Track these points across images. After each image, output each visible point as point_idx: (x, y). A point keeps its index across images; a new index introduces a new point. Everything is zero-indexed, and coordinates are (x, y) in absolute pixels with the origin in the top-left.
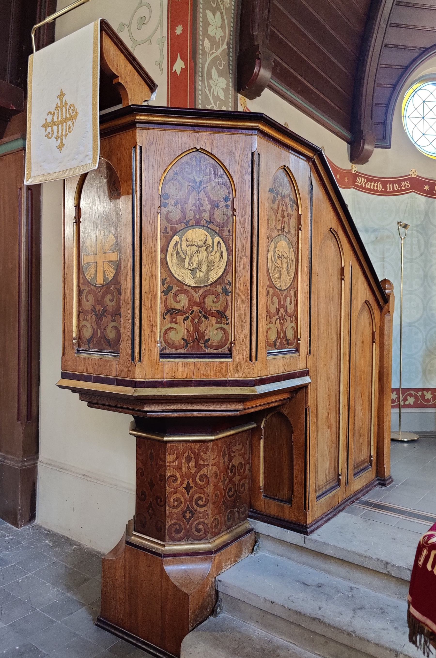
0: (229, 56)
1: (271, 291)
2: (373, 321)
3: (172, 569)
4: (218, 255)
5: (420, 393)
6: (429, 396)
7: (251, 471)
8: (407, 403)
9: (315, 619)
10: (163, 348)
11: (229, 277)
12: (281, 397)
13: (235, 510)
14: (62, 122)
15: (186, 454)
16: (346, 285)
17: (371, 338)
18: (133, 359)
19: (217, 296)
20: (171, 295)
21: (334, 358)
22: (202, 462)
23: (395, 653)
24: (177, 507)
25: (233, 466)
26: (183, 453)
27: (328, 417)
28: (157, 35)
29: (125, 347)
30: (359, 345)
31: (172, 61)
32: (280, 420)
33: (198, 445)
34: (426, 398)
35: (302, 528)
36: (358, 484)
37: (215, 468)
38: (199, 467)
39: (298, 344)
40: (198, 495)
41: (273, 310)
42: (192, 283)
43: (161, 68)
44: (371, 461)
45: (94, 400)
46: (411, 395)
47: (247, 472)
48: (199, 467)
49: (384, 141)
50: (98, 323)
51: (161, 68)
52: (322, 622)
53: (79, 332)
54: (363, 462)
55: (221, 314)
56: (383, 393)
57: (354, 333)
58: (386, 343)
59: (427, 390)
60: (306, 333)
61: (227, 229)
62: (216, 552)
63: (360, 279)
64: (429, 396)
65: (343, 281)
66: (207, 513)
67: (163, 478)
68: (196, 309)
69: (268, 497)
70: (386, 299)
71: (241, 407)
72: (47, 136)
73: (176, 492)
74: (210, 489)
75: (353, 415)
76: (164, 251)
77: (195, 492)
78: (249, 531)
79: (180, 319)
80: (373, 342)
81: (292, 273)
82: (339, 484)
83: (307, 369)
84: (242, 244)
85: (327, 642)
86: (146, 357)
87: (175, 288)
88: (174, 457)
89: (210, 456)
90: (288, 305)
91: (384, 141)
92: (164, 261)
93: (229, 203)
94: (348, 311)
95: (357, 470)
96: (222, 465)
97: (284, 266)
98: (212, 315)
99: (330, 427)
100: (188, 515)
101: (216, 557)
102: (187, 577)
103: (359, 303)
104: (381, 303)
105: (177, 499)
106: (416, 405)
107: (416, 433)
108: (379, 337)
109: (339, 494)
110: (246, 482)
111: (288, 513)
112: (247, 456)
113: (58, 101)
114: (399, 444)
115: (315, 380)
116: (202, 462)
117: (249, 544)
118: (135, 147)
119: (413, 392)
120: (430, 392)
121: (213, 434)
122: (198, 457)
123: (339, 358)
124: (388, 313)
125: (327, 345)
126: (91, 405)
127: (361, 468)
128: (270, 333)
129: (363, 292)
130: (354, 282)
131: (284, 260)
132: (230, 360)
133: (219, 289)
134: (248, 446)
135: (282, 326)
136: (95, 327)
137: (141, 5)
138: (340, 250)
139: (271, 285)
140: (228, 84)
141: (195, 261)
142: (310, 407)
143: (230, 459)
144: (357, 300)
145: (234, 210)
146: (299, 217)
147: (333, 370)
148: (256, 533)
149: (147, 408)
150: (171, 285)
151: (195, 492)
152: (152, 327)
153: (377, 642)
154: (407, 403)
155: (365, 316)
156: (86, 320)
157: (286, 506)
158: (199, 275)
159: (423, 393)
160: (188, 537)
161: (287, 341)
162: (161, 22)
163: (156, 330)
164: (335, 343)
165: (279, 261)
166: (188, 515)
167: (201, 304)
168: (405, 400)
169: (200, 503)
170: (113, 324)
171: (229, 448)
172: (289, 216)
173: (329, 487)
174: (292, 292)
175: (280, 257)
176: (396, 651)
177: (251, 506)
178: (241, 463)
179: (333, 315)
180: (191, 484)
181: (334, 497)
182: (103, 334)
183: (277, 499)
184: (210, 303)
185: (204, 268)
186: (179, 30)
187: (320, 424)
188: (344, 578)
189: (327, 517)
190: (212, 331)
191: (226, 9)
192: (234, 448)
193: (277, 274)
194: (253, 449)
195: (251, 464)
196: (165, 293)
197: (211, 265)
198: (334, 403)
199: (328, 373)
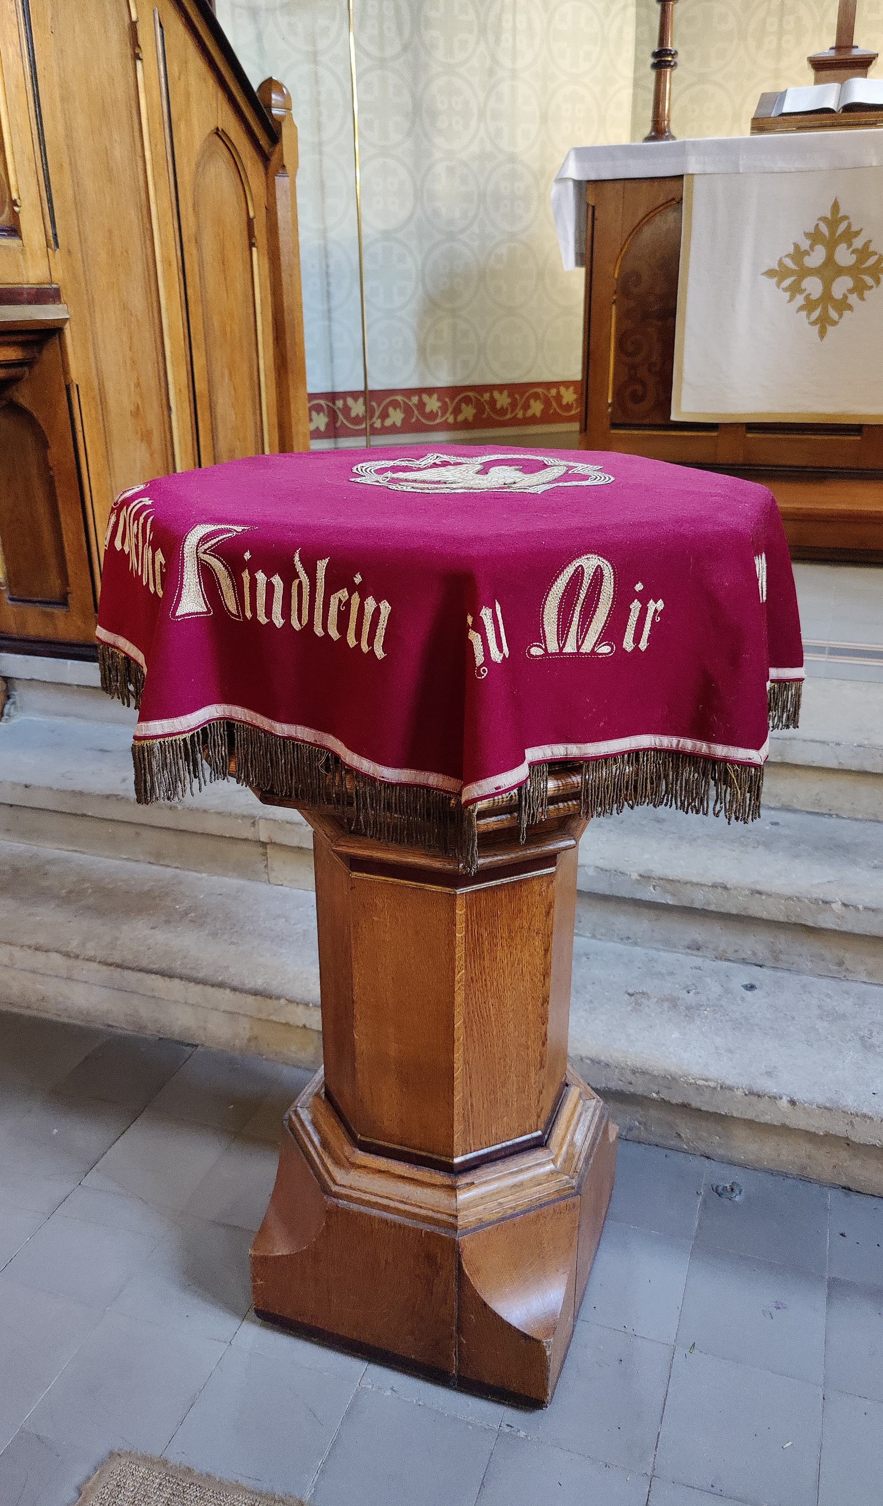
2: (246, 188)
5: (415, 399)
6: (433, 404)
8: (388, 422)
9: (108, 797)
16: (148, 72)
17: (245, 233)
21: (138, 269)
23: (252, 821)
27: (137, 413)
34: (428, 410)
46: (395, 404)
52: (122, 798)
56: (286, 372)
57: (190, 210)
59: (430, 391)
60: (34, 189)
63: (191, 65)
65: (139, 63)
69: (19, 601)
75: (207, 414)
80: (252, 245)
83: (54, 286)
85: (138, 834)
94: (163, 148)
99: (146, 437)
104: (263, 141)
108: (266, 234)
119: (399, 398)
120: (435, 396)
123: (152, 273)
125: (110, 232)
129: (204, 108)
142: (76, 382)
144: (188, 122)
147: (138, 300)
153: (221, 810)
154: (388, 422)
155: (220, 174)
157: (58, 611)
159: (420, 400)
168: (385, 415)
176: (253, 817)
179: (120, 153)
183: (39, 602)
199: (125, 307)
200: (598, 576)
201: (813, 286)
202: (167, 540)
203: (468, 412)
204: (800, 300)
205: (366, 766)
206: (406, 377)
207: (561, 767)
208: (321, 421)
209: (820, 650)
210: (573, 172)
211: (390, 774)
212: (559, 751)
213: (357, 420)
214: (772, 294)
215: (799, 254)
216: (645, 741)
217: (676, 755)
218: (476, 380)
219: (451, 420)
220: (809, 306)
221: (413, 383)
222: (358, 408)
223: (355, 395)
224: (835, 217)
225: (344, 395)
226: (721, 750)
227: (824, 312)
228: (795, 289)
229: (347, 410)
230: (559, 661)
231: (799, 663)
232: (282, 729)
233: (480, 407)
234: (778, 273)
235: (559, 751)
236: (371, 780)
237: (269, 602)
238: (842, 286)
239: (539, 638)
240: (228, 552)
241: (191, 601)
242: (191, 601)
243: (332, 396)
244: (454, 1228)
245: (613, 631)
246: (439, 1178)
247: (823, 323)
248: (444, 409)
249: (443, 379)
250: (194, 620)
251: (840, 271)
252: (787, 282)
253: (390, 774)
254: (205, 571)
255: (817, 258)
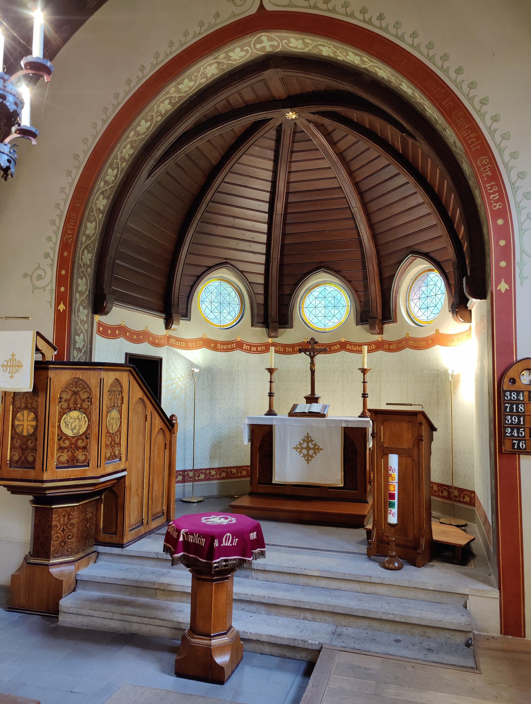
0: (89, 297)
1: (108, 435)
3: (54, 571)
4: (84, 422)
5: (208, 471)
7: (96, 521)
10: (57, 465)
11: (89, 432)
12: (112, 482)
13: (87, 541)
14: (12, 366)
15: (63, 514)
18: (43, 470)
19: (83, 440)
20: (62, 441)
22: (71, 517)
24: (57, 540)
25: (87, 518)
26: (62, 513)
27: (137, 490)
28: (49, 287)
29: (38, 465)
30: (156, 452)
31: (58, 304)
32: (112, 494)
33: (70, 509)
35: (121, 546)
36: (154, 525)
37: (77, 520)
38: (69, 519)
39: (121, 457)
40: (68, 534)
41: (108, 443)
42: (72, 435)
43: (51, 305)
44: (163, 513)
45: (14, 490)
46: (202, 473)
47: (94, 521)
48: (69, 519)
49: (186, 315)
50: (23, 454)
51: (51, 305)
53: (11, 457)
54: (158, 513)
55: (84, 448)
58: (173, 449)
59: (212, 469)
61: (88, 411)
62: (77, 561)
64: (213, 472)
66: (73, 542)
67: (50, 527)
68: (73, 446)
70: (173, 425)
71: (93, 488)
72: (4, 370)
73: (57, 533)
74: (75, 530)
76: (59, 421)
77: (67, 532)
78: (95, 551)
79: (66, 451)
81: (119, 424)
82: (143, 524)
84: (95, 417)
86: (49, 469)
87: (64, 438)
88: (57, 516)
89: (75, 514)
90: (116, 440)
91: (186, 315)
92: (59, 426)
93: (90, 400)
95: (153, 518)
96: (81, 518)
97: (115, 422)
98: (80, 448)
99: (138, 495)
100: (63, 544)
101: (77, 563)
102: (62, 572)
103: (156, 429)
104: (170, 428)
105: (58, 537)
106: (205, 479)
107: (202, 496)
109: (142, 530)
110: (93, 526)
111: (115, 539)
112: (94, 513)
113: (11, 357)
114: (192, 504)
115: (130, 474)
116: (71, 517)
117: (94, 558)
118: (47, 378)
121: (77, 502)
122: (69, 515)
124: (174, 433)
126: (13, 493)
127: (157, 516)
128: (107, 454)
130: (153, 420)
131: (115, 419)
132: (88, 468)
133: (84, 437)
134: (95, 508)
135: (113, 450)
136: (21, 455)
137: (39, 268)
138: (145, 406)
139: (108, 432)
140: (88, 312)
141: (73, 425)
143: (86, 515)
145: (91, 402)
146: (123, 398)
147: (140, 466)
148: (98, 553)
149: (47, 492)
150: (62, 436)
151: (67, 532)
152: (52, 456)
154: (200, 478)
155: (161, 436)
156: (15, 452)
157: (114, 536)
158: (75, 431)
160: (62, 555)
161: (115, 456)
162: (51, 281)
163: (54, 456)
164: (142, 453)
165: (112, 421)
166: (63, 544)
167: (76, 444)
168: (199, 476)
169: (69, 537)
170: (32, 454)
171: (85, 510)
172: (117, 399)
173: (136, 526)
174: (118, 433)
175: (112, 419)
177: (96, 539)
178: (91, 517)
180: (65, 528)
181: (139, 531)
182: (26, 459)
184: (80, 443)
185: (77, 428)
186: (62, 289)
187: (132, 494)
188: (139, 565)
189: (134, 541)
190: (81, 456)
191: (88, 274)
192: (87, 509)
193: (111, 427)
194: (98, 510)
195: (96, 517)
196: (59, 440)
197: (80, 427)
198: (140, 483)
200: (229, 536)
201: (305, 451)
202: (179, 532)
203: (224, 475)
204: (302, 455)
205: (201, 560)
206: (206, 465)
207: (225, 561)
208: (180, 478)
209: (268, 545)
210: (247, 422)
211: (204, 561)
212: (225, 558)
213: (191, 478)
214: (295, 453)
215: (301, 444)
216: (236, 557)
217: (240, 559)
218: (226, 466)
219: (218, 477)
220: (304, 456)
221: (208, 467)
222: (191, 474)
223: (191, 471)
224: (308, 437)
225: (188, 471)
226: (246, 558)
227: (308, 458)
228: (300, 452)
229: (188, 475)
230: (225, 546)
231: (264, 548)
232: (191, 555)
233: (227, 473)
234: (296, 448)
235: (225, 558)
236: (202, 562)
237: (191, 539)
238: (311, 452)
239: (222, 543)
240: (186, 533)
241: (181, 539)
242: (181, 539)
243: (184, 471)
244: (211, 646)
245: (232, 543)
246: (209, 638)
247: (308, 461)
248: (216, 474)
249: (216, 465)
250: (182, 541)
251: (311, 449)
252: (299, 450)
253: (204, 561)
254: (183, 535)
255: (305, 445)
